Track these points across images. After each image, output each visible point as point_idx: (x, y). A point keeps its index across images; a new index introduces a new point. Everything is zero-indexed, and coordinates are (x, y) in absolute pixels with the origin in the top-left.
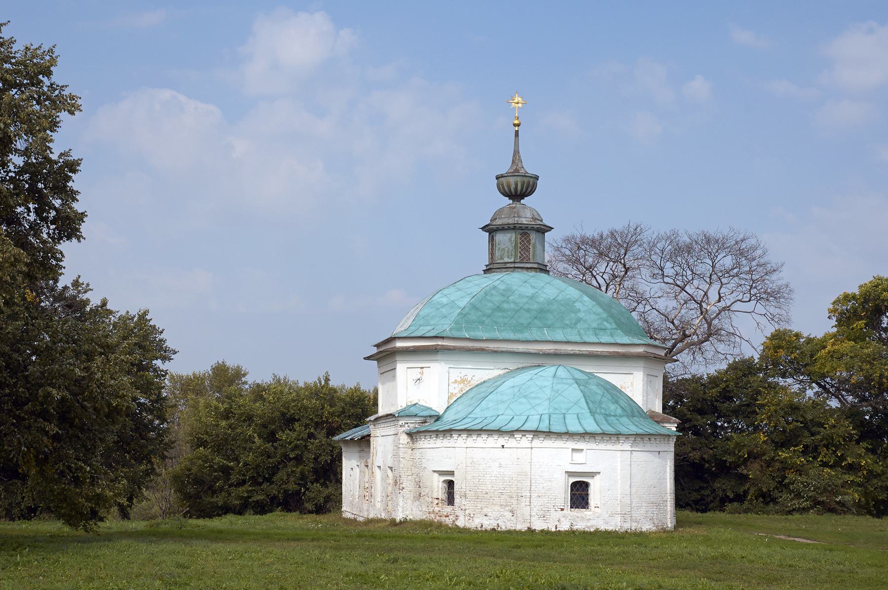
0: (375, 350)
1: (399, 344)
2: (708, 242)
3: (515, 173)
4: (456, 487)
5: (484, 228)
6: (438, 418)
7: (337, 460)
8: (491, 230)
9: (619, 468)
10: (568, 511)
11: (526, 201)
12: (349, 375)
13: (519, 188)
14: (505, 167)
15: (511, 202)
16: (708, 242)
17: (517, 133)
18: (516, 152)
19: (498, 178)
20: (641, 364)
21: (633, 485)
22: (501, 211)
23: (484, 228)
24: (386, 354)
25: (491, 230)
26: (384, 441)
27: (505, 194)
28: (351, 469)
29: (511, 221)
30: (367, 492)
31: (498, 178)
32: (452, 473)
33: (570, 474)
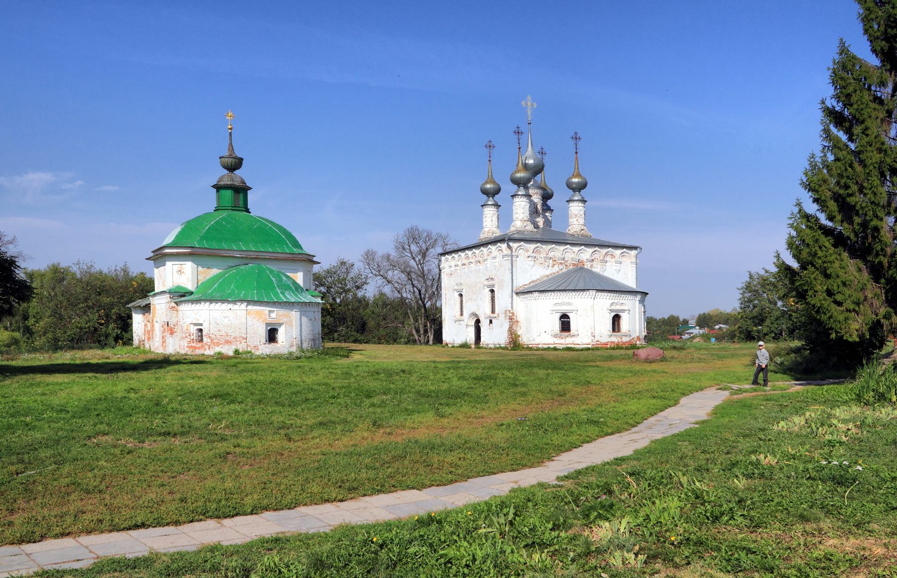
0: (152, 254)
1: (167, 251)
2: (715, 414)
3: (230, 156)
4: (204, 333)
5: (213, 186)
6: (192, 293)
7: (130, 317)
8: (218, 188)
9: (679, 381)
10: (267, 345)
11: (236, 172)
12: (138, 266)
13: (235, 165)
16: (715, 414)
18: (231, 144)
19: (220, 158)
20: (190, 258)
21: (295, 330)
22: (223, 176)
23: (213, 186)
24: (159, 256)
25: (218, 188)
26: (160, 304)
27: (224, 167)
28: (138, 320)
29: (229, 183)
30: (149, 334)
31: (220, 158)
32: (201, 325)
33: (267, 324)
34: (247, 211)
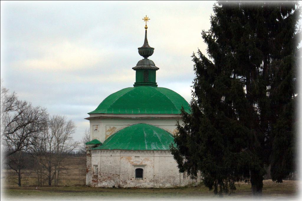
0: (89, 116)
11: (150, 58)
14: (141, 45)
15: (144, 58)
17: (146, 31)
34: (155, 85)
